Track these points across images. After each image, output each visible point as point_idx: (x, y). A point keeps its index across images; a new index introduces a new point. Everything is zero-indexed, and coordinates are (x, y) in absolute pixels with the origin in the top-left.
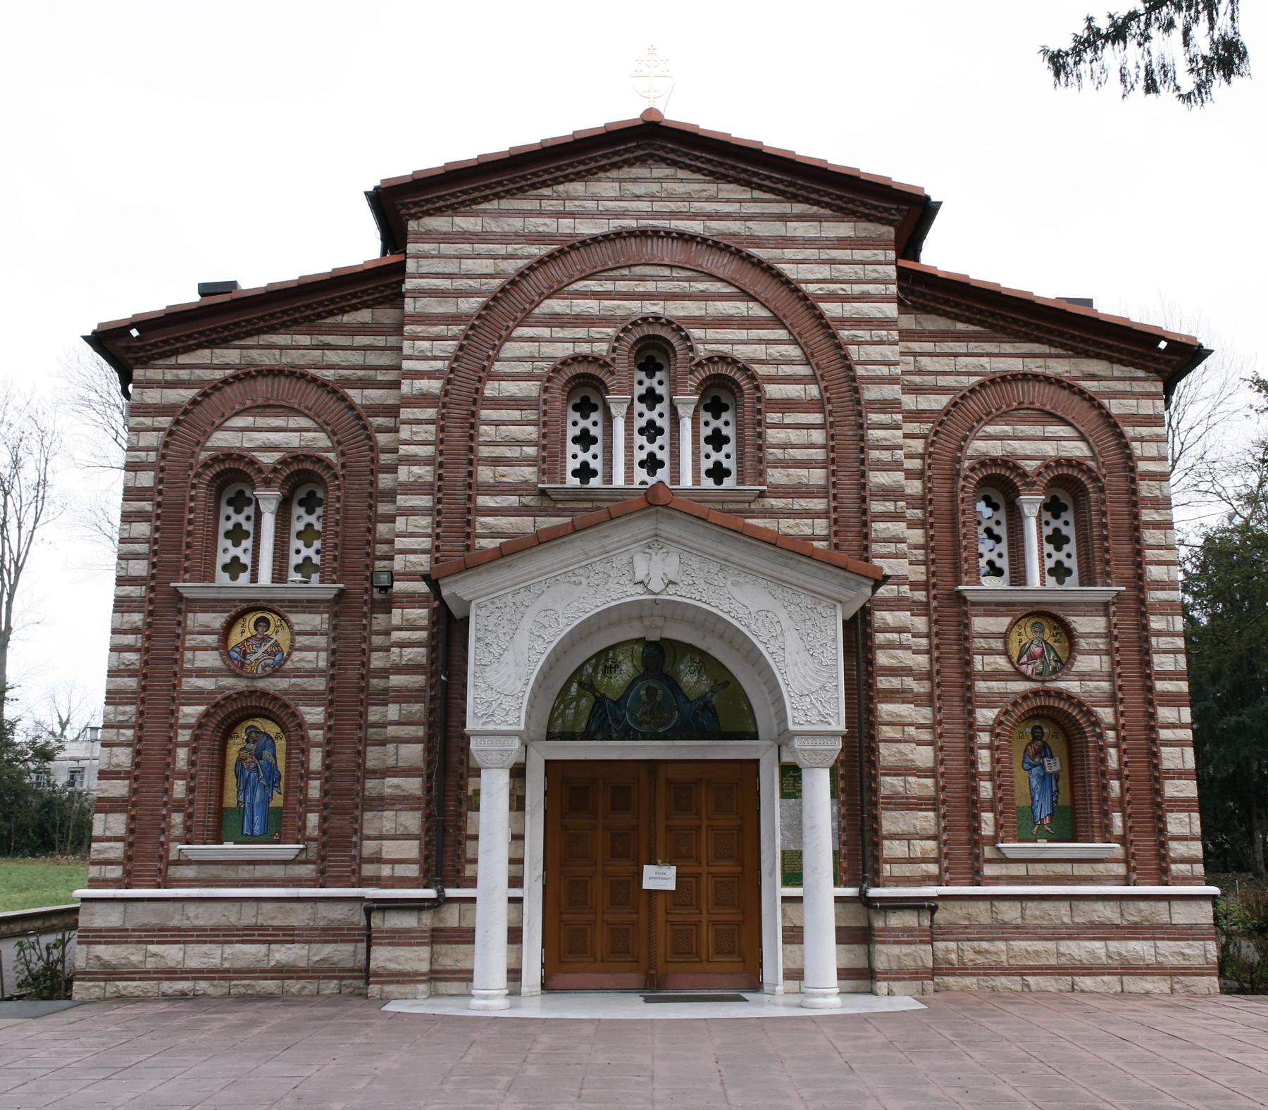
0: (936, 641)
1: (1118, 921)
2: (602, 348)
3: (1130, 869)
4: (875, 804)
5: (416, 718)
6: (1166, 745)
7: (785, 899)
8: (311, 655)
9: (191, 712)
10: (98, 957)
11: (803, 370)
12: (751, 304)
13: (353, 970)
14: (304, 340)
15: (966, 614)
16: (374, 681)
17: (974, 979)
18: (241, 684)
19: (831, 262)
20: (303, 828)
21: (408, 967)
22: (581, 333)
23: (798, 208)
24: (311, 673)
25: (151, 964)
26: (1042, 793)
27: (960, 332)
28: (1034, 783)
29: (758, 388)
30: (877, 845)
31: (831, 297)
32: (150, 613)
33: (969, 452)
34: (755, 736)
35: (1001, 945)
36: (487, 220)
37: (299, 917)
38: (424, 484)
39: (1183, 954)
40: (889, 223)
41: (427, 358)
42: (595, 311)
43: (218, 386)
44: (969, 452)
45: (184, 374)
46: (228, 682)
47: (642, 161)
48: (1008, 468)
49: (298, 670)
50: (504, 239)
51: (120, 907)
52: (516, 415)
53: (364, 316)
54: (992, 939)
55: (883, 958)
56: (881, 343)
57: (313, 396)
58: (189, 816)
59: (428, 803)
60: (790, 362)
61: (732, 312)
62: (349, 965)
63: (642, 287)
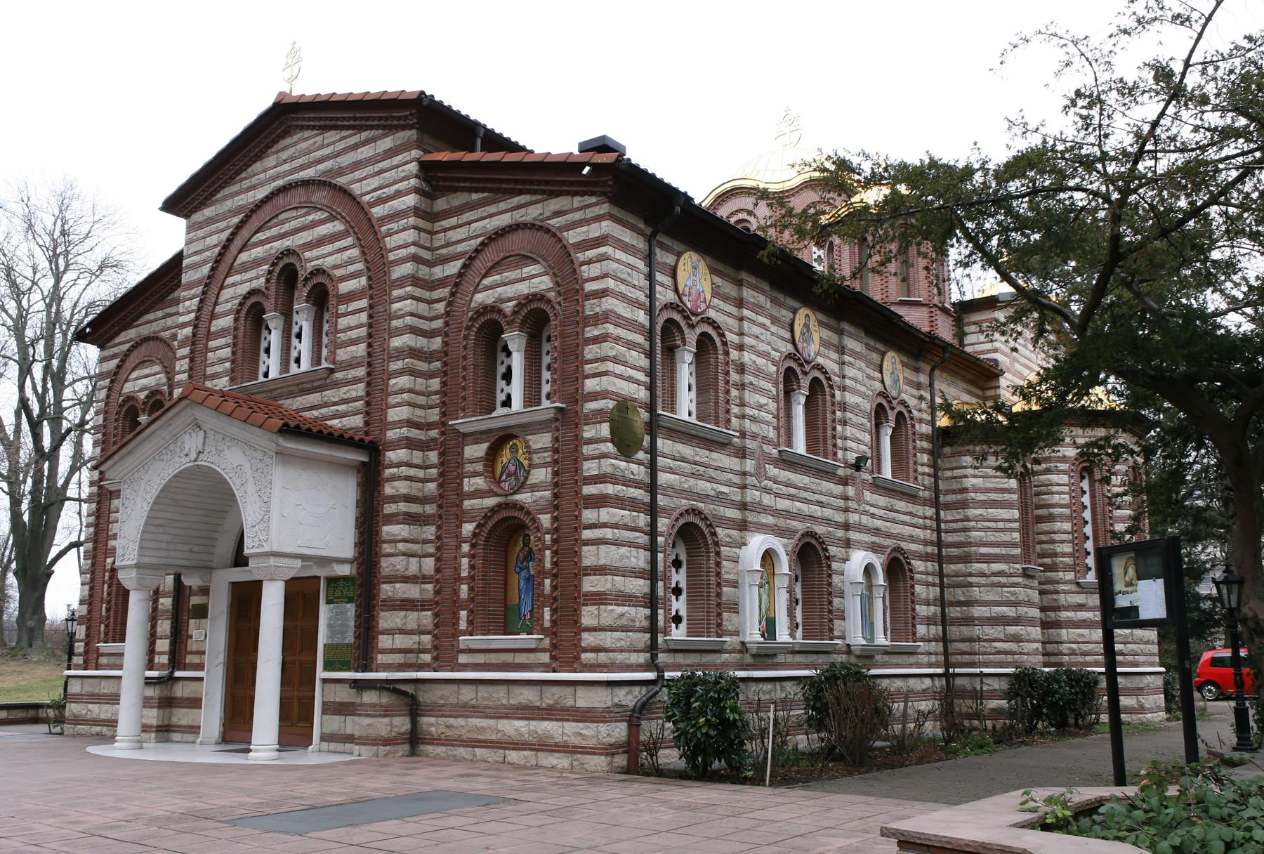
1: (538, 704)
3: (552, 658)
6: (587, 544)
7: (325, 681)
9: (468, 528)
14: (160, 314)
17: (443, 749)
19: (381, 172)
26: (526, 593)
28: (522, 583)
30: (375, 638)
35: (461, 721)
39: (581, 734)
40: (410, 127)
43: (127, 355)
47: (286, 133)
48: (482, 314)
54: (456, 717)
63: (286, 227)
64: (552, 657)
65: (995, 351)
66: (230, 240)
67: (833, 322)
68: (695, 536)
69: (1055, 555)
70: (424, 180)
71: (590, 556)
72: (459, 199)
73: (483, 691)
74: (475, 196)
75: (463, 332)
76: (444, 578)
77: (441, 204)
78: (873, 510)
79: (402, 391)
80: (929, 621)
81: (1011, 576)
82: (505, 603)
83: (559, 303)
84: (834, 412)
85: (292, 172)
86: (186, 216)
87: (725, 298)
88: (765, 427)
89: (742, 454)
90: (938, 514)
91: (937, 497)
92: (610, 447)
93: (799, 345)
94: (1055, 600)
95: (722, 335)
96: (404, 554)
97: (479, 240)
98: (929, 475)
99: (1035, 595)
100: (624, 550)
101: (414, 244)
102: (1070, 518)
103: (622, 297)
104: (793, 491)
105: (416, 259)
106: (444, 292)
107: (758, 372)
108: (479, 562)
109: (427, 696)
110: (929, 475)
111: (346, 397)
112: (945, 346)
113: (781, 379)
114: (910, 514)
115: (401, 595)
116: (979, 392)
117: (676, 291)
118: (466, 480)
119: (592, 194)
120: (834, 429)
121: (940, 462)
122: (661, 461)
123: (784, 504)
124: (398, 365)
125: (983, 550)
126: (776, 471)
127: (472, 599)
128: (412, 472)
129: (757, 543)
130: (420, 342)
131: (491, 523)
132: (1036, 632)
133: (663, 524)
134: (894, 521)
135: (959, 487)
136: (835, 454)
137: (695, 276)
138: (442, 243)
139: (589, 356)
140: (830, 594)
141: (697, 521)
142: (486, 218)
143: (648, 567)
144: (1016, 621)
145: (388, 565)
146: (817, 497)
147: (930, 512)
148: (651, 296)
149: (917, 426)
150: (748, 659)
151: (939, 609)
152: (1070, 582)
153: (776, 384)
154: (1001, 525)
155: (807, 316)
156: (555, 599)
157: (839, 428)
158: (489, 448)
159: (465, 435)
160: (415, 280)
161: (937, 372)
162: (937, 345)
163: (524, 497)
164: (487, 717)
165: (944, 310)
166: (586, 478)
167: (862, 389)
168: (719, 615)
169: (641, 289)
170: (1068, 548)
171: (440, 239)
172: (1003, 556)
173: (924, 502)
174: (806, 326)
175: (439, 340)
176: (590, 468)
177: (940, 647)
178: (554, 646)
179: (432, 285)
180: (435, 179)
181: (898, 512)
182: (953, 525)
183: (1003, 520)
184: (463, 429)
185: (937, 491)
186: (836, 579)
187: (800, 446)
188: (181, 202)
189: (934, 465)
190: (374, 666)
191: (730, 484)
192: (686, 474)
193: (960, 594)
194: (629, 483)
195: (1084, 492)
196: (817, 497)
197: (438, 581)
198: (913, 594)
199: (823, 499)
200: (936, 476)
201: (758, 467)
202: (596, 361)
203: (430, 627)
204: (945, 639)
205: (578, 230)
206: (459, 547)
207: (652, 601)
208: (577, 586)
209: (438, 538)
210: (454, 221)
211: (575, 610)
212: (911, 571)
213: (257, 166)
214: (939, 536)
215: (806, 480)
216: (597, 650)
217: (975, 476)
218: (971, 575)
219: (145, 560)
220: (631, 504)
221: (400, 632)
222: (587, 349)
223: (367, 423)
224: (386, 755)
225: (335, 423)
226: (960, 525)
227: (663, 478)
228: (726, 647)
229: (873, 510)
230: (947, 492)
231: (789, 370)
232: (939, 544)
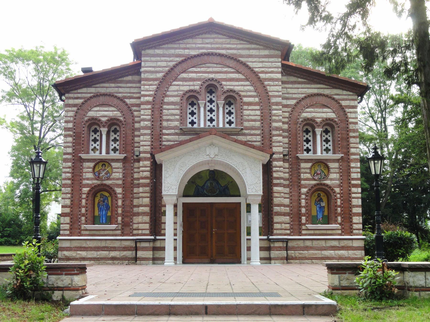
0: (291, 170)
1: (338, 246)
2: (197, 88)
3: (342, 232)
4: (272, 214)
5: (147, 191)
8: (118, 174)
9: (85, 190)
10: (64, 255)
11: (255, 94)
12: (239, 75)
13: (132, 258)
14: (113, 85)
15: (299, 162)
16: (135, 181)
18: (99, 182)
19: (262, 62)
20: (117, 221)
21: (147, 256)
22: (191, 83)
23: (253, 46)
24: (118, 179)
25: (78, 256)
26: (320, 212)
27: (300, 81)
28: (318, 209)
29: (241, 99)
31: (262, 72)
32: (73, 163)
33: (301, 116)
34: (239, 196)
35: (306, 252)
36: (164, 50)
37: (117, 244)
38: (148, 127)
41: (148, 91)
42: (195, 77)
44: (301, 116)
45: (79, 95)
46: (95, 182)
49: (114, 178)
50: (169, 56)
51: (69, 242)
52: (173, 107)
53: (129, 78)
55: (273, 254)
56: (276, 85)
57: (116, 101)
58: (86, 218)
59: (151, 214)
60: (250, 91)
61: (234, 77)
62: (131, 257)
74: (300, 80)
111: (250, 140)
145: (276, 201)
163: (328, 182)
184: (300, 158)
213: (190, 40)
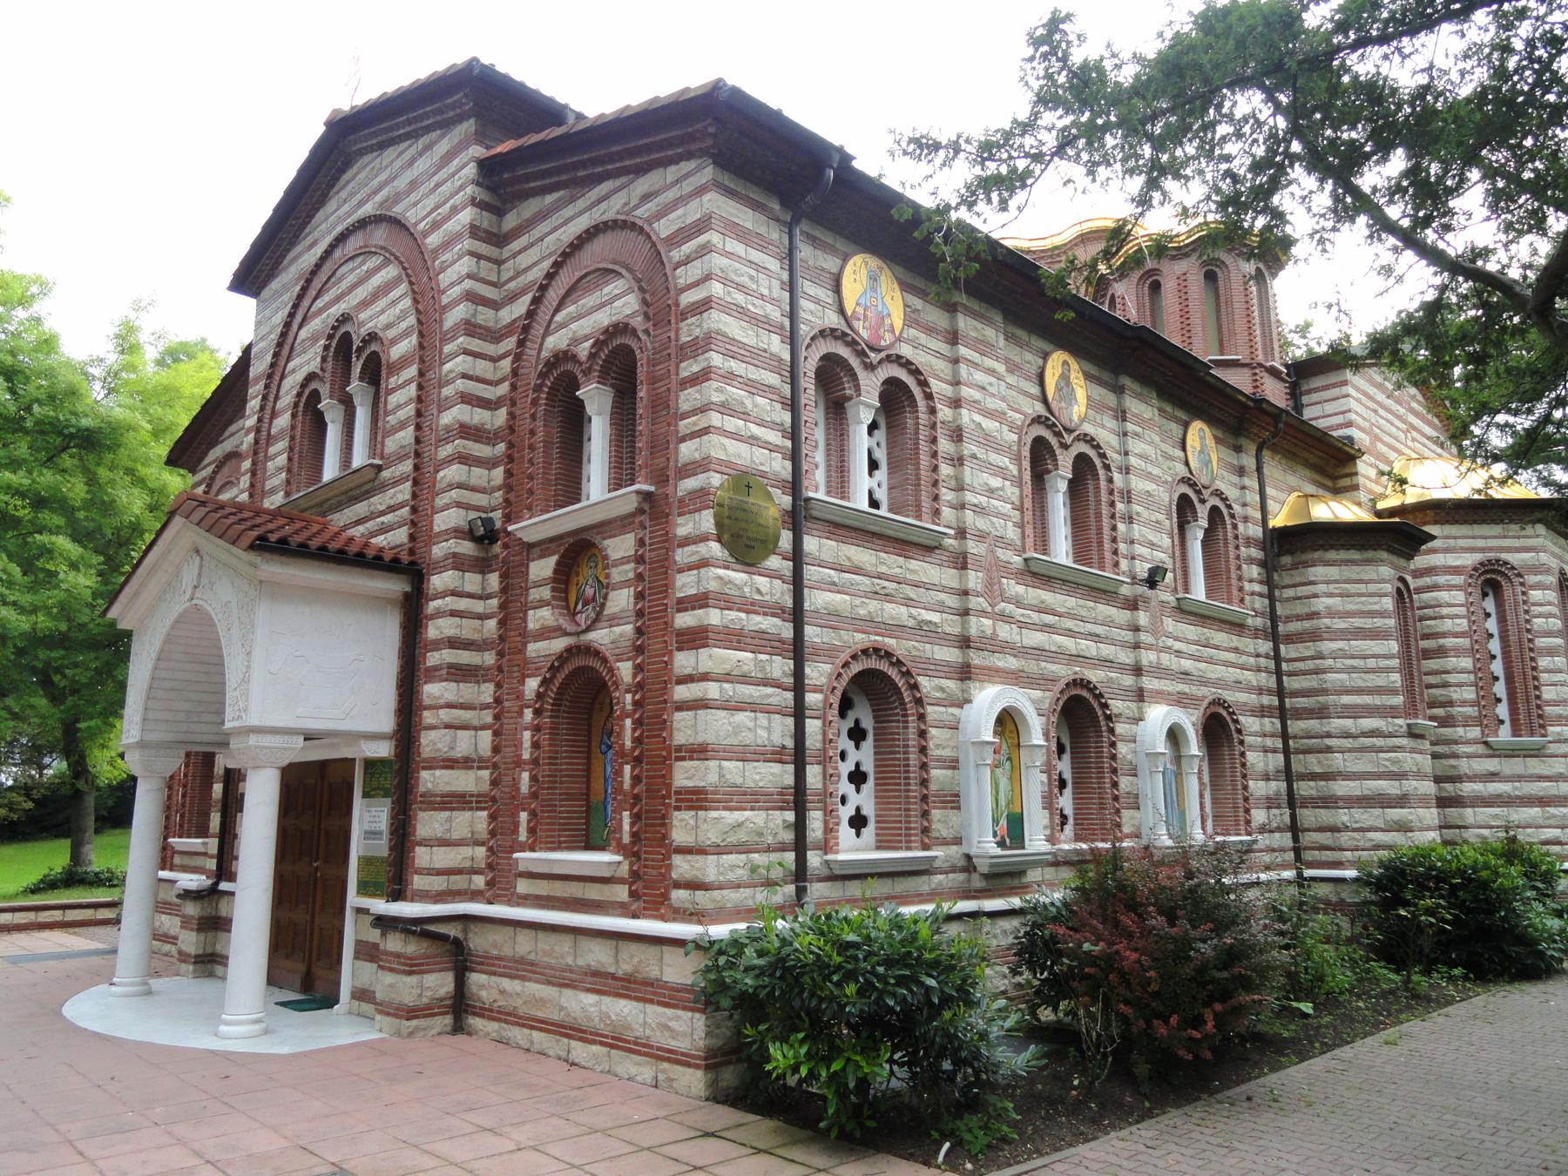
1: (612, 970)
3: (633, 894)
9: (532, 684)
39: (668, 1028)
43: (212, 478)
54: (511, 977)
64: (632, 894)
65: (1349, 424)
66: (291, 315)
67: (1106, 376)
68: (878, 692)
69: (1450, 703)
70: (488, 188)
71: (684, 728)
72: (531, 207)
73: (546, 942)
75: (531, 396)
76: (499, 763)
77: (510, 221)
78: (1178, 645)
79: (451, 487)
80: (1270, 803)
81: (1391, 735)
82: (588, 800)
83: (646, 332)
84: (1112, 504)
85: (349, 214)
86: (255, 295)
87: (930, 330)
88: (998, 522)
89: (961, 562)
90: (1276, 649)
91: (1274, 626)
92: (715, 549)
93: (1054, 405)
94: (1453, 767)
95: (923, 384)
96: (447, 727)
97: (552, 260)
98: (1261, 595)
99: (1426, 762)
100: (743, 717)
101: (469, 276)
102: (1472, 652)
103: (742, 313)
104: (1048, 619)
105: (471, 297)
106: (510, 343)
107: (988, 441)
108: (544, 738)
109: (479, 941)
110: (1261, 595)
112: (1275, 414)
113: (1026, 452)
114: (1236, 650)
115: (444, 788)
116: (1329, 484)
117: (842, 311)
118: (531, 612)
119: (689, 156)
120: (1114, 528)
121: (1276, 577)
122: (811, 572)
123: (1035, 638)
124: (445, 451)
125: (1346, 699)
126: (1020, 589)
127: (534, 795)
128: (464, 604)
129: (988, 699)
130: (479, 416)
131: (560, 677)
132: (1431, 815)
133: (817, 672)
134: (1210, 661)
135: (1306, 610)
136: (1116, 564)
137: (870, 293)
138: (511, 273)
139: (685, 407)
140: (1114, 771)
141: (883, 666)
142: (561, 225)
143: (790, 743)
144: (1402, 801)
145: (431, 742)
146: (1090, 627)
147: (1266, 646)
148: (793, 315)
149: (1241, 527)
150: (978, 883)
151: (1283, 785)
152: (1475, 742)
153: (1018, 459)
154: (1371, 663)
155: (1065, 363)
156: (637, 798)
157: (1121, 527)
158: (558, 563)
159: (531, 546)
160: (471, 328)
161: (1266, 453)
162: (1265, 412)
164: (549, 983)
165: (1273, 372)
166: (680, 601)
167: (1156, 471)
168: (925, 814)
169: (773, 301)
170: (1469, 694)
171: (508, 270)
172: (1377, 708)
173: (1257, 633)
174: (1065, 377)
175: (503, 411)
176: (685, 584)
177: (1286, 839)
178: (635, 875)
179: (495, 336)
180: (503, 184)
181: (1216, 647)
182: (1300, 665)
183: (1373, 656)
185: (1274, 617)
186: (1123, 749)
187: (1062, 551)
188: (251, 277)
189: (1268, 582)
190: (409, 894)
191: (941, 608)
192: (856, 597)
193: (1313, 763)
194: (750, 607)
195: (1488, 615)
196: (1090, 627)
197: (495, 766)
198: (1243, 765)
199: (1099, 630)
200: (1271, 597)
201: (990, 584)
202: (694, 412)
203: (484, 835)
204: (1295, 829)
205: (672, 216)
206: (521, 714)
207: (798, 799)
208: (667, 777)
209: (498, 701)
210: (523, 240)
211: (664, 817)
212: (1239, 731)
213: (320, 215)
214: (1280, 682)
215: (1071, 602)
216: (695, 885)
217: (1330, 595)
218: (1329, 735)
219: (152, 737)
220: (761, 642)
221: (449, 839)
222: (683, 395)
223: (412, 538)
224: (411, 1034)
225: (380, 541)
226: (1310, 665)
227: (816, 600)
228: (937, 864)
229: (1178, 645)
230: (1289, 619)
231: (1039, 442)
232: (1281, 692)
